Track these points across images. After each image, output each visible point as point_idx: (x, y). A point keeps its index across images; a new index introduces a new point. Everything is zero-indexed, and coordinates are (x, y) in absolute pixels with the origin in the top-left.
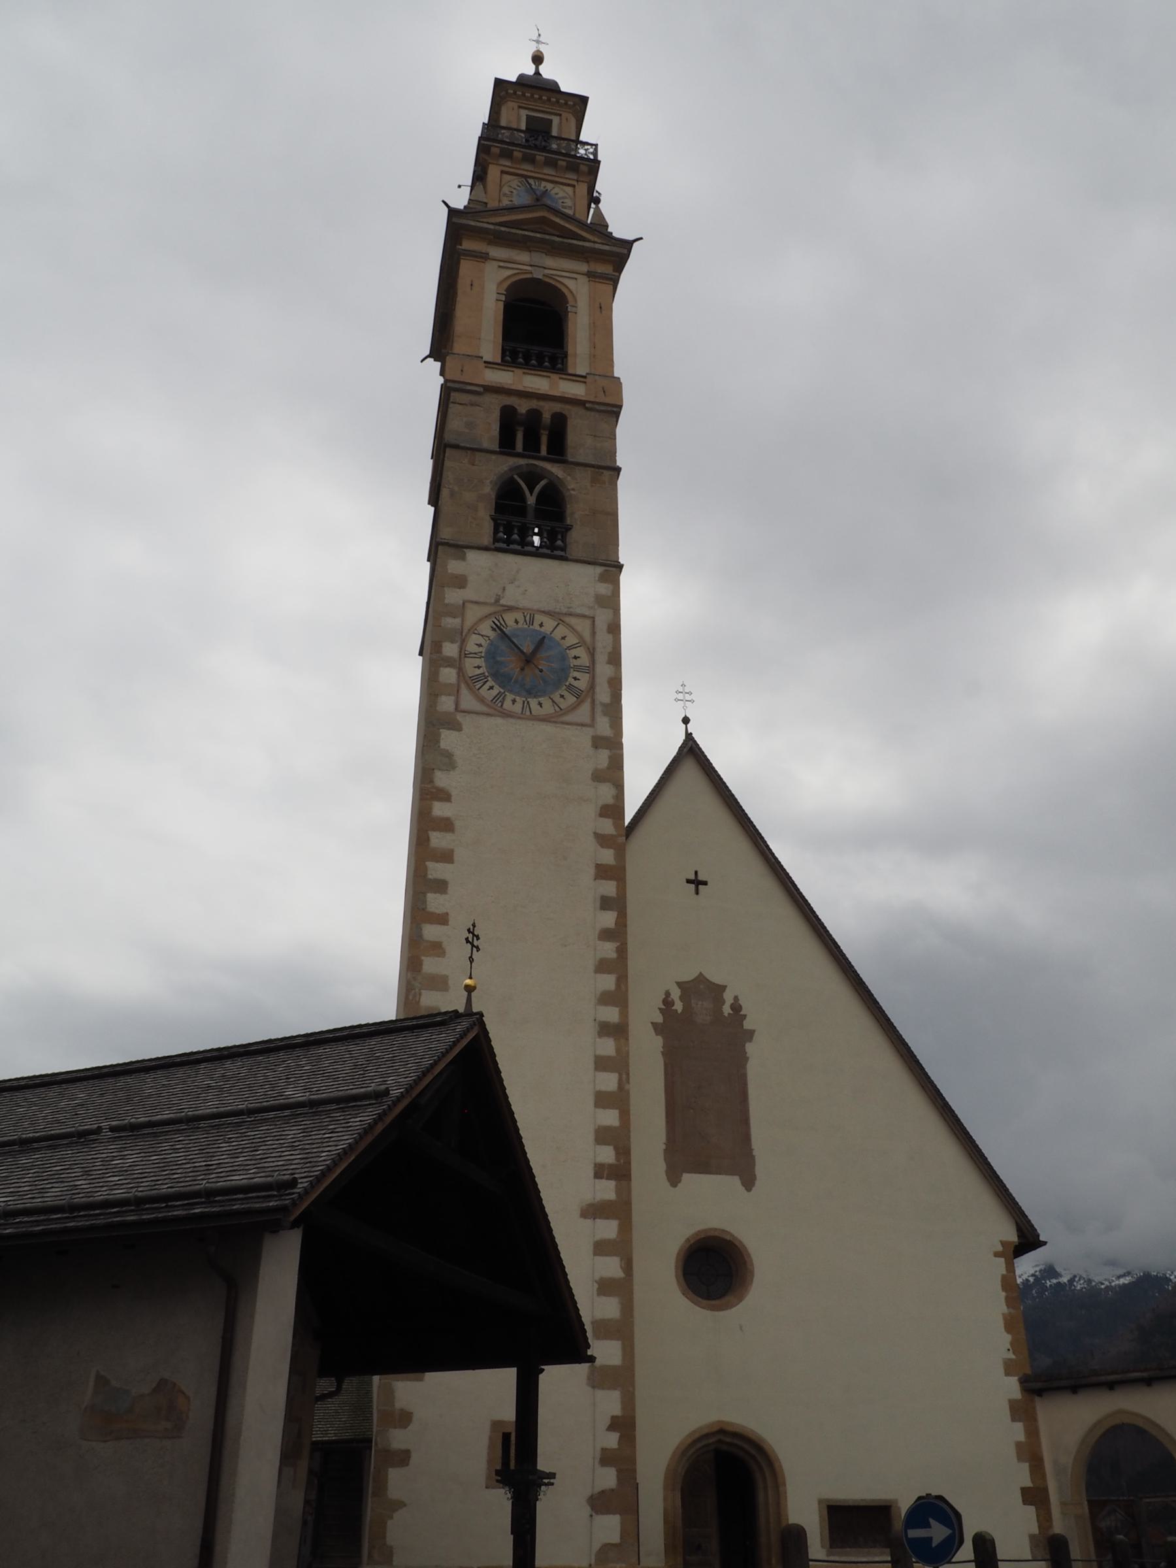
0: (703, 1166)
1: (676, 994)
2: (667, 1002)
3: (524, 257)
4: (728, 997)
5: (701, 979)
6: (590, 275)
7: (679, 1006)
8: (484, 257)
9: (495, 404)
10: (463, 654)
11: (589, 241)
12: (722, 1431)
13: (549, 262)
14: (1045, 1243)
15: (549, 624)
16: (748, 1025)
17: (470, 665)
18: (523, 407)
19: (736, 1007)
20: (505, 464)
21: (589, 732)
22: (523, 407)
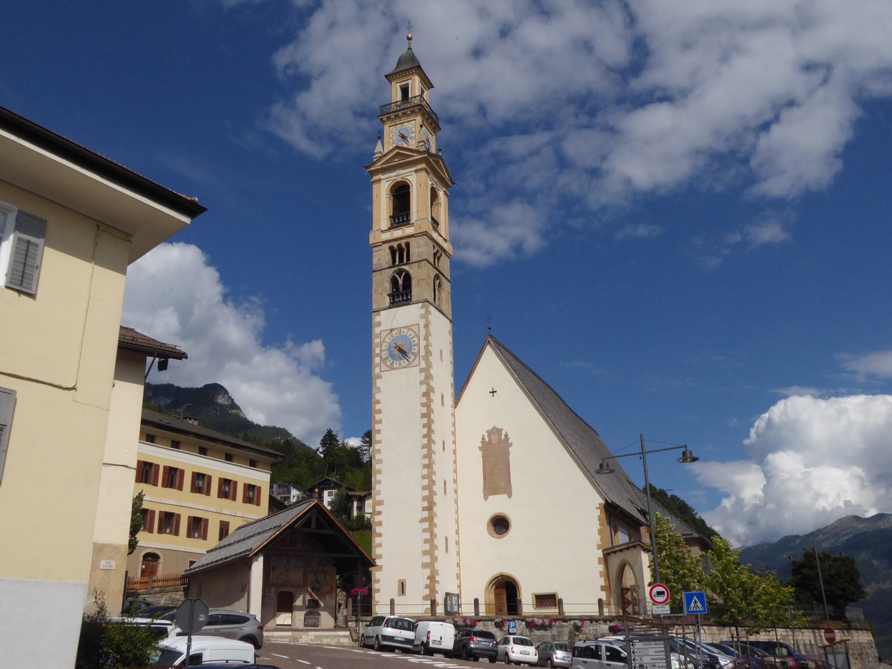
0: (495, 493)
1: (486, 435)
2: (483, 439)
3: (394, 174)
4: (503, 433)
5: (494, 428)
6: (416, 171)
7: (487, 439)
8: (380, 180)
9: (387, 246)
10: (381, 351)
11: (412, 156)
12: (502, 576)
13: (402, 172)
14: (486, 498)
15: (406, 331)
16: (510, 441)
17: (384, 355)
18: (395, 244)
19: (506, 436)
20: (390, 272)
21: (418, 368)
22: (395, 244)
